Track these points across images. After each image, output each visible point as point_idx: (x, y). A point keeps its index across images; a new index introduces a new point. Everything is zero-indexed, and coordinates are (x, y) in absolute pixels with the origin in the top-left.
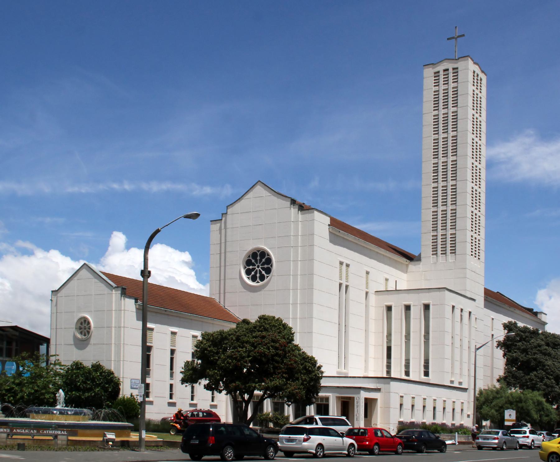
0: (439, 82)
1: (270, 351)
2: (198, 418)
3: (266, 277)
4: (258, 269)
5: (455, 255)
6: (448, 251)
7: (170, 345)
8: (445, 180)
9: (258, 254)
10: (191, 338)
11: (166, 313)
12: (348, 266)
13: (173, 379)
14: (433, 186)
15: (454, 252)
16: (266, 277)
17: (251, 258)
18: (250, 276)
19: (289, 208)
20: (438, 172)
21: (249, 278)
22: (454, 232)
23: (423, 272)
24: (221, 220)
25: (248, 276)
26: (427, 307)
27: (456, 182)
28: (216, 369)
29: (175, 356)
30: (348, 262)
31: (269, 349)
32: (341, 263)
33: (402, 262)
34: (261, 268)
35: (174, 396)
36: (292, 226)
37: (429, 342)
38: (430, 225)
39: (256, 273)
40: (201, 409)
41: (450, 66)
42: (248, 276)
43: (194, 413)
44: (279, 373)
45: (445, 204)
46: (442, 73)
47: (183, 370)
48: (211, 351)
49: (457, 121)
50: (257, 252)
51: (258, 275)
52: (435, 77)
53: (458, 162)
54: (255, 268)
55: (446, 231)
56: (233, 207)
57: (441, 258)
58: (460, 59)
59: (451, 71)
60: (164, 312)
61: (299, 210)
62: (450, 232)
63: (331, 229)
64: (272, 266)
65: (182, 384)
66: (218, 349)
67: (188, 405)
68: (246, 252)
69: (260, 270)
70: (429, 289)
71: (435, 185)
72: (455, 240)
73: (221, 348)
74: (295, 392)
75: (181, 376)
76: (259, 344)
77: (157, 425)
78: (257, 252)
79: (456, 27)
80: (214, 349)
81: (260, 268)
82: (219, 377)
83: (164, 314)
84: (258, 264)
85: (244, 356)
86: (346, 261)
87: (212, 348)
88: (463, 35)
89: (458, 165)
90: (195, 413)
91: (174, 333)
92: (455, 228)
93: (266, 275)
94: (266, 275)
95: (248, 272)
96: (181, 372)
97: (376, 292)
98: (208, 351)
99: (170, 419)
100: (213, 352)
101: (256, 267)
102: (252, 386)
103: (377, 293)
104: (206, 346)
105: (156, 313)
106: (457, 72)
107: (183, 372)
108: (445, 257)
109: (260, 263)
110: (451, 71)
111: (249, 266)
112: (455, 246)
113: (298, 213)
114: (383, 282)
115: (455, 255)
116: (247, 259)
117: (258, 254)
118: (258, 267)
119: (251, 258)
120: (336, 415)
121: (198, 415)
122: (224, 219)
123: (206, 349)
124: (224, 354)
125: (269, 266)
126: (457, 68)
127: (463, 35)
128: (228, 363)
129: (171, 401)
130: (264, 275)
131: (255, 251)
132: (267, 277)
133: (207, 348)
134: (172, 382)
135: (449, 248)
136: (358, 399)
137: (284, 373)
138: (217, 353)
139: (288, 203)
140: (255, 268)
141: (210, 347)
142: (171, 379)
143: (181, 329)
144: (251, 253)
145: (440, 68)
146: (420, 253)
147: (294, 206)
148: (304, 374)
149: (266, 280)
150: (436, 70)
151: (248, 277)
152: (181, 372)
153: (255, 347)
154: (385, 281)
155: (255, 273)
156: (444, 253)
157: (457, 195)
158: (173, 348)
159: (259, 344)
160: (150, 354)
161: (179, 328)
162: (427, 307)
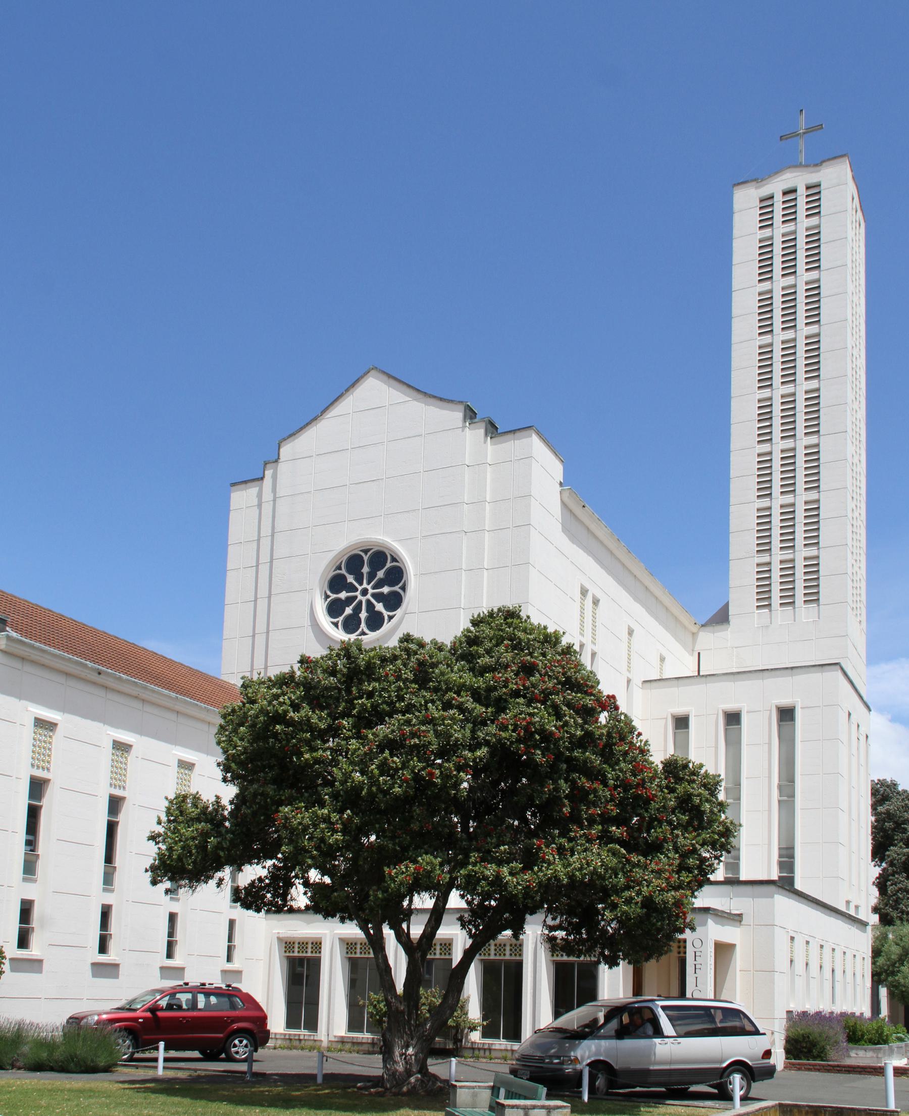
0: (772, 218)
1: (566, 724)
2: (195, 1014)
3: (386, 618)
4: (364, 599)
5: (818, 605)
6: (800, 597)
7: (109, 781)
8: (790, 433)
9: (366, 558)
10: (176, 769)
11: (100, 679)
12: (596, 602)
13: (112, 891)
14: (758, 451)
15: (813, 597)
16: (386, 618)
17: (343, 571)
18: (341, 619)
19: (461, 429)
20: (771, 418)
21: (336, 625)
22: (815, 553)
23: (735, 650)
24: (262, 478)
25: (335, 620)
26: (786, 714)
27: (819, 437)
28: (322, 805)
29: (122, 818)
30: (599, 595)
31: (559, 716)
32: (584, 592)
33: (686, 623)
34: (373, 595)
35: (112, 945)
36: (467, 476)
37: (794, 801)
38: (751, 540)
39: (358, 609)
40: (204, 984)
41: (798, 179)
42: (335, 620)
43: (178, 996)
44: (592, 822)
45: (789, 488)
46: (779, 198)
47: (160, 829)
48: (305, 725)
49: (819, 301)
50: (363, 554)
51: (363, 615)
52: (761, 208)
53: (822, 393)
54: (356, 597)
55: (794, 552)
56: (296, 441)
57: (780, 614)
58: (824, 164)
59: (802, 192)
60: (94, 677)
61: (486, 435)
62: (801, 553)
63: (566, 495)
64: (404, 588)
65: (154, 883)
66: (334, 717)
67: (158, 973)
68: (331, 556)
69: (368, 601)
70: (792, 668)
71: (765, 448)
72: (818, 571)
73: (346, 714)
74: (671, 901)
75: (151, 852)
76: (516, 694)
77: (43, 1044)
78: (363, 554)
79: (801, 111)
80: (319, 719)
81: (360, 588)
82: (339, 836)
83: (94, 683)
84: (365, 585)
85: (457, 740)
86: (593, 590)
87: (306, 710)
88: (820, 127)
89: (822, 400)
90: (184, 998)
91: (121, 747)
92: (818, 543)
93: (386, 614)
94: (386, 614)
95: (334, 609)
96: (153, 838)
97: (645, 682)
98: (289, 723)
99: (96, 1018)
100: (311, 728)
101: (358, 593)
102: (485, 878)
103: (648, 684)
104: (281, 704)
105: (67, 675)
106: (819, 193)
107: (159, 835)
108: (792, 611)
109: (369, 583)
110: (802, 192)
111: (338, 592)
112: (818, 586)
113: (485, 442)
114: (656, 662)
115: (818, 605)
116: (332, 574)
117: (366, 558)
118: (365, 592)
119: (343, 571)
120: (712, 997)
121: (194, 1004)
122: (269, 473)
123: (279, 718)
124: (359, 736)
125: (396, 588)
126: (818, 185)
127: (820, 127)
128: (384, 768)
129: (102, 958)
130: (380, 614)
131: (356, 552)
132: (390, 618)
133: (286, 712)
134: (108, 899)
135: (800, 592)
136: (697, 943)
137: (606, 820)
138: (334, 731)
139: (456, 415)
140: (356, 597)
141: (296, 707)
142: (105, 890)
143: (144, 738)
144: (346, 558)
145: (776, 186)
146: (728, 602)
147: (472, 425)
148: (685, 827)
149: (386, 627)
150: (765, 191)
151: (333, 623)
152: (153, 838)
153: (500, 706)
154: (659, 662)
155: (354, 610)
156: (789, 601)
157: (822, 469)
158: (118, 792)
159: (516, 694)
160: (41, 807)
161: (138, 736)
162: (786, 714)
